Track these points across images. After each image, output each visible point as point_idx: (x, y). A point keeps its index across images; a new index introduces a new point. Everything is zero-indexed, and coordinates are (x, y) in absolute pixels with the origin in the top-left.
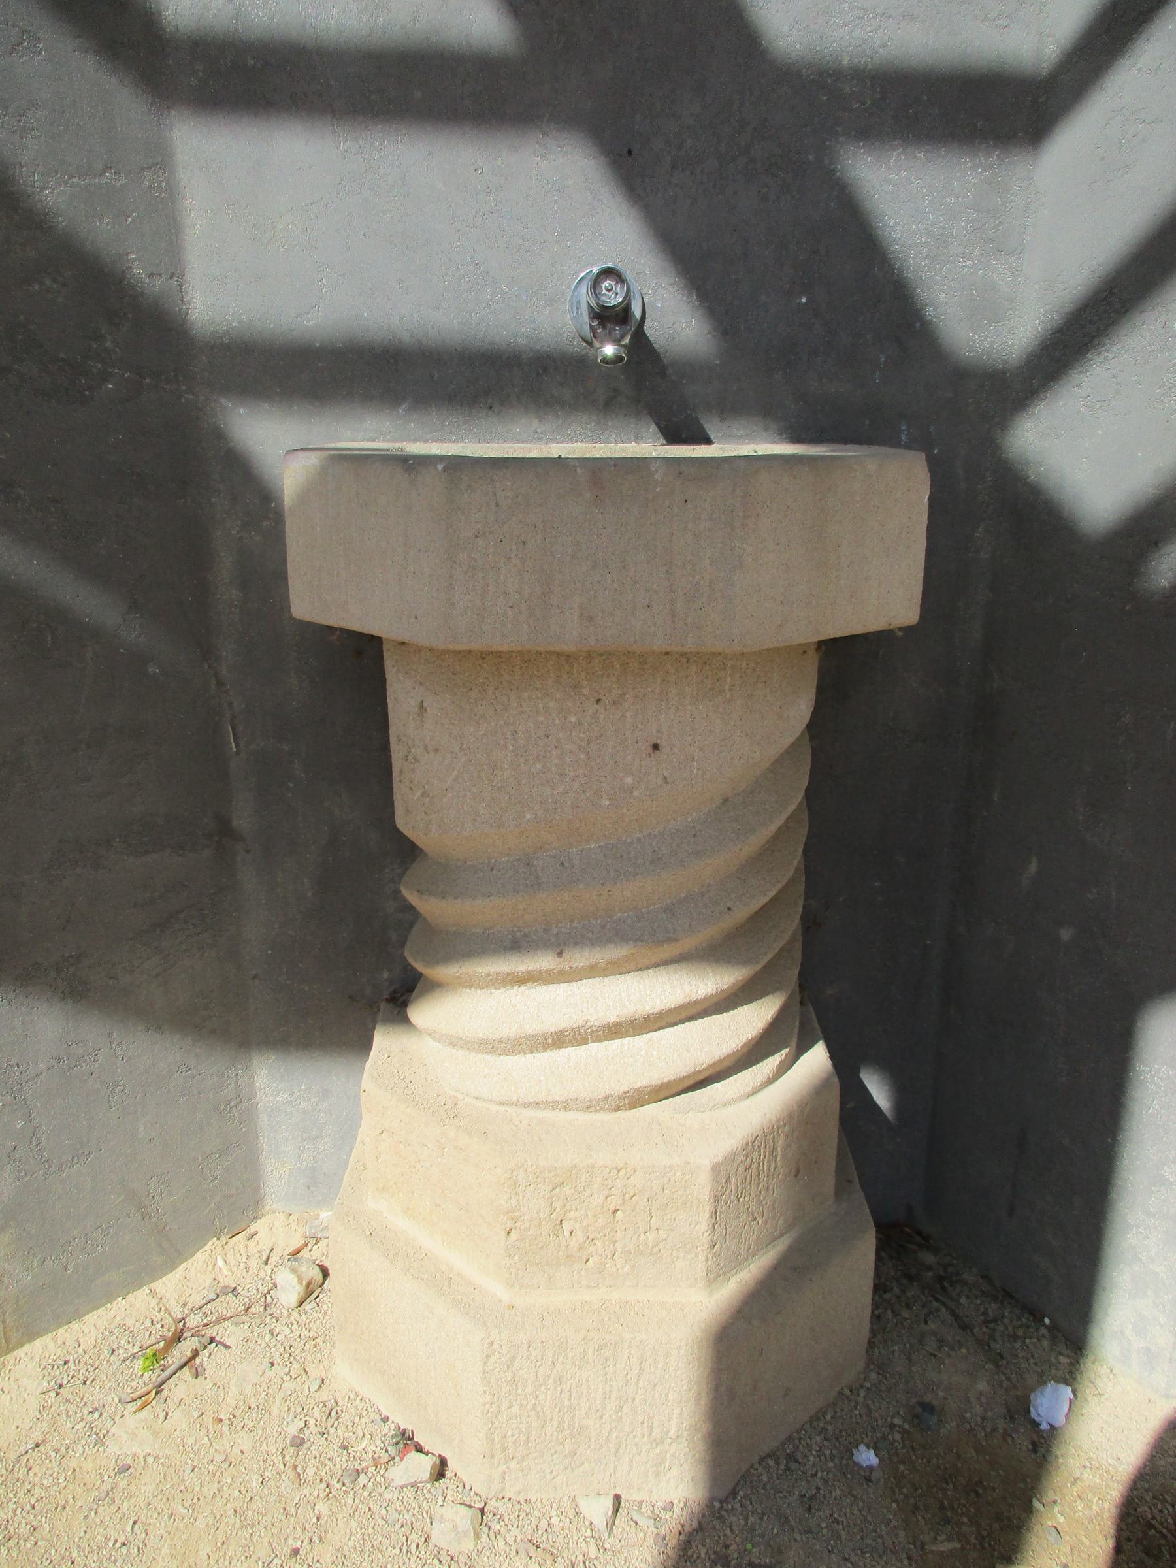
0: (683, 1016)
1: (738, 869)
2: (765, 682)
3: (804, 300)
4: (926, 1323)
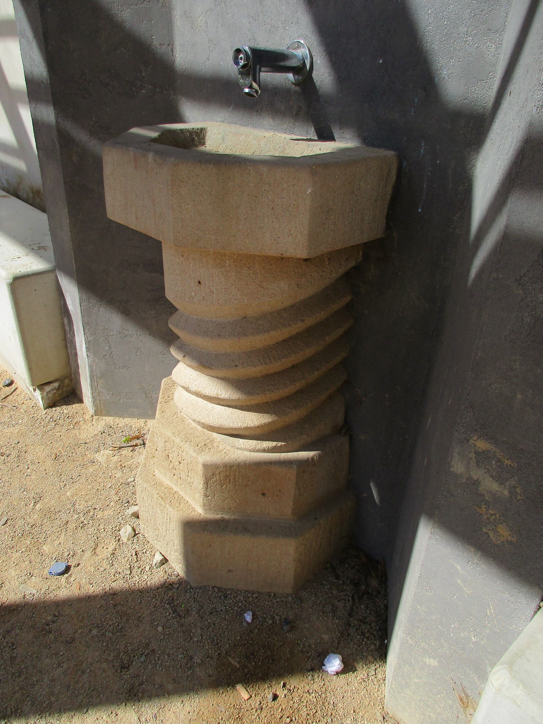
0: (228, 404)
1: (250, 351)
2: (249, 268)
3: (381, 61)
4: (339, 601)
